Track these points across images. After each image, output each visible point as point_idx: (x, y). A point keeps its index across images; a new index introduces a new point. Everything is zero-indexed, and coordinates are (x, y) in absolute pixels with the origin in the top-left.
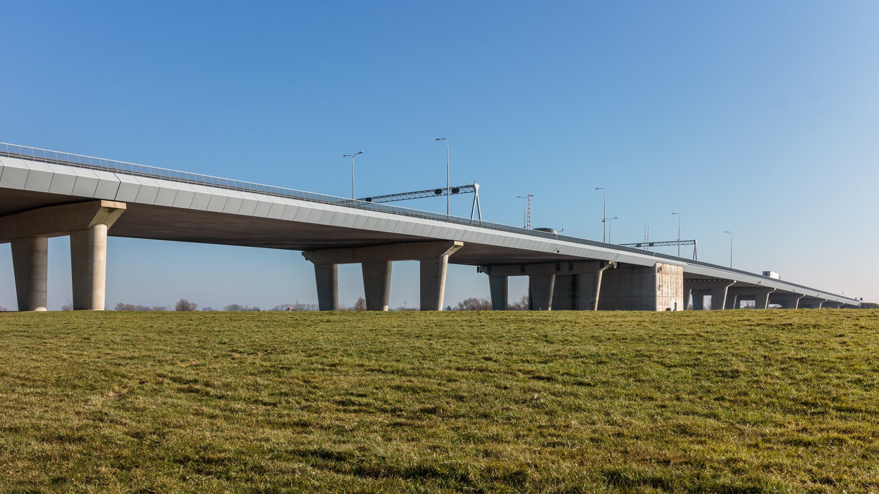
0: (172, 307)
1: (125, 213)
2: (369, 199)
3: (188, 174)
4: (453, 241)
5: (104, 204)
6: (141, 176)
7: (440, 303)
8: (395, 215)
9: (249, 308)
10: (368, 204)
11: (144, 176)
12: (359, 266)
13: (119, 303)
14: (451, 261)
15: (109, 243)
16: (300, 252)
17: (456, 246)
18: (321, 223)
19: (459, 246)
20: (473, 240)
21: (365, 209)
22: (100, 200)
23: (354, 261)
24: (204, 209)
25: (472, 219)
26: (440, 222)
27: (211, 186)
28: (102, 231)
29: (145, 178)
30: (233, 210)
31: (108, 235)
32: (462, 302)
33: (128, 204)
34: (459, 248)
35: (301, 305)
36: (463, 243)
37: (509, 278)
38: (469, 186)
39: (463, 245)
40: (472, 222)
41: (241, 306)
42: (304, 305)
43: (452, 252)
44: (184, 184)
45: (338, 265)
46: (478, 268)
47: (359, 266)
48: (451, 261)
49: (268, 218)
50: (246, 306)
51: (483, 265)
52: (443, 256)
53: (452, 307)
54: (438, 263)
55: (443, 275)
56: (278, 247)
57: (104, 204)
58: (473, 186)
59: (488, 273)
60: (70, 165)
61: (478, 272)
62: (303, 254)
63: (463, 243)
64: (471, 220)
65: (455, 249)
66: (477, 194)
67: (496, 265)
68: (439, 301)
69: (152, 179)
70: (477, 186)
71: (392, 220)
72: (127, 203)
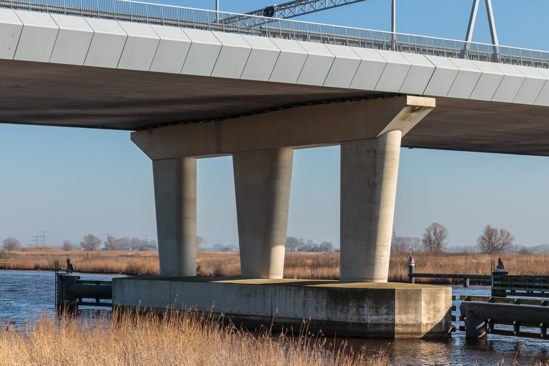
0: (61, 245)
1: (434, 112)
2: (269, 11)
4: (403, 96)
5: (411, 101)
6: (62, 13)
7: (379, 249)
8: (381, 51)
10: (270, 21)
12: (228, 161)
13: (87, 235)
14: (407, 143)
15: (401, 153)
17: (414, 109)
18: (538, 103)
19: (421, 108)
21: (263, 33)
23: (219, 151)
25: (470, 41)
26: (405, 54)
27: (28, 9)
29: (70, 17)
34: (426, 113)
35: (403, 239)
36: (434, 100)
39: (434, 105)
41: (301, 239)
42: (409, 239)
43: (409, 126)
47: (228, 161)
50: (309, 241)
52: (386, 134)
54: (375, 152)
56: (48, 122)
57: (411, 101)
60: (84, 15)
63: (434, 100)
64: (392, 34)
65: (414, 115)
68: (378, 243)
72: (437, 98)
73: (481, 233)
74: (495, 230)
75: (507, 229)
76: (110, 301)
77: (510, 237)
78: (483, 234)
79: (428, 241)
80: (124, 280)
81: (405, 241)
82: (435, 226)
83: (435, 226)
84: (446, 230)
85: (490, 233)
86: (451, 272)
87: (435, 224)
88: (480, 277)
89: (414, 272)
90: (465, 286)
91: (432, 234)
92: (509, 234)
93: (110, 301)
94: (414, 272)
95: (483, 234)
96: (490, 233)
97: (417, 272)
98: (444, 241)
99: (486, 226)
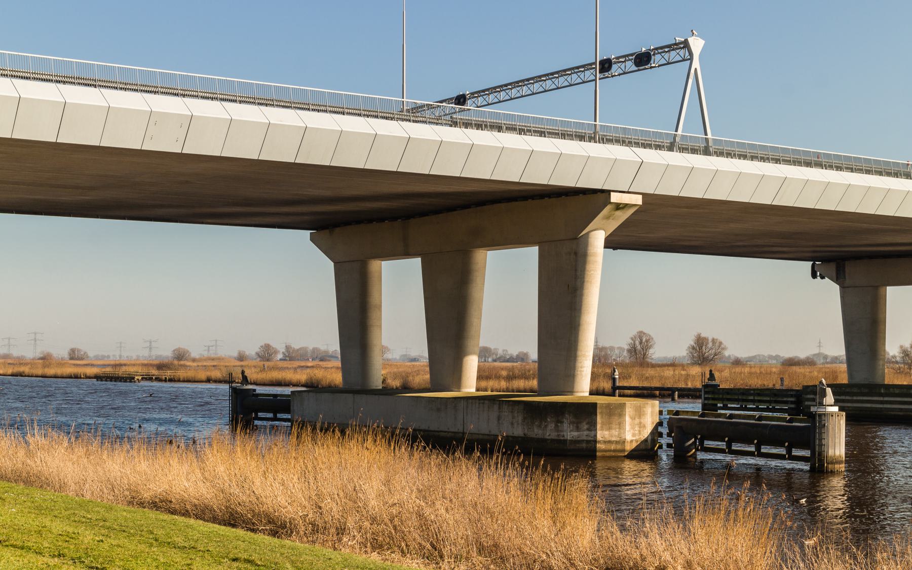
2: (461, 100)
3: (854, 157)
4: (607, 193)
5: (615, 198)
6: (235, 101)
9: (509, 352)
10: (461, 111)
11: (240, 102)
13: (263, 344)
14: (612, 243)
15: (605, 256)
16: (307, 234)
17: (619, 207)
20: (672, 190)
22: (608, 192)
23: (407, 253)
24: (426, 172)
25: (680, 132)
26: (609, 146)
28: (598, 238)
29: (243, 106)
30: (695, 191)
31: (605, 247)
32: (280, 347)
33: (644, 195)
36: (640, 196)
37: (889, 289)
38: (676, 44)
40: (678, 139)
41: (495, 349)
42: (612, 348)
43: (613, 225)
44: (321, 114)
45: (383, 263)
46: (813, 266)
48: (612, 243)
49: (655, 194)
50: (504, 350)
51: (826, 260)
52: (588, 234)
53: (657, 353)
54: (576, 254)
55: (587, 285)
57: (615, 198)
58: (686, 45)
59: (838, 278)
61: (814, 276)
62: (313, 239)
63: (640, 196)
65: (618, 213)
66: (696, 64)
67: (858, 257)
69: (178, 99)
70: (697, 44)
71: (767, 175)
73: (691, 342)
74: (706, 339)
75: (720, 338)
76: (288, 416)
77: (722, 346)
78: (692, 343)
79: (633, 351)
80: (304, 393)
81: (608, 350)
82: (641, 334)
83: (641, 334)
84: (652, 338)
85: (700, 342)
86: (658, 385)
87: (641, 332)
88: (690, 389)
89: (618, 384)
90: (673, 400)
91: (637, 343)
92: (721, 343)
93: (288, 416)
94: (618, 384)
95: (692, 343)
96: (700, 342)
97: (621, 385)
98: (651, 351)
99: (696, 334)
